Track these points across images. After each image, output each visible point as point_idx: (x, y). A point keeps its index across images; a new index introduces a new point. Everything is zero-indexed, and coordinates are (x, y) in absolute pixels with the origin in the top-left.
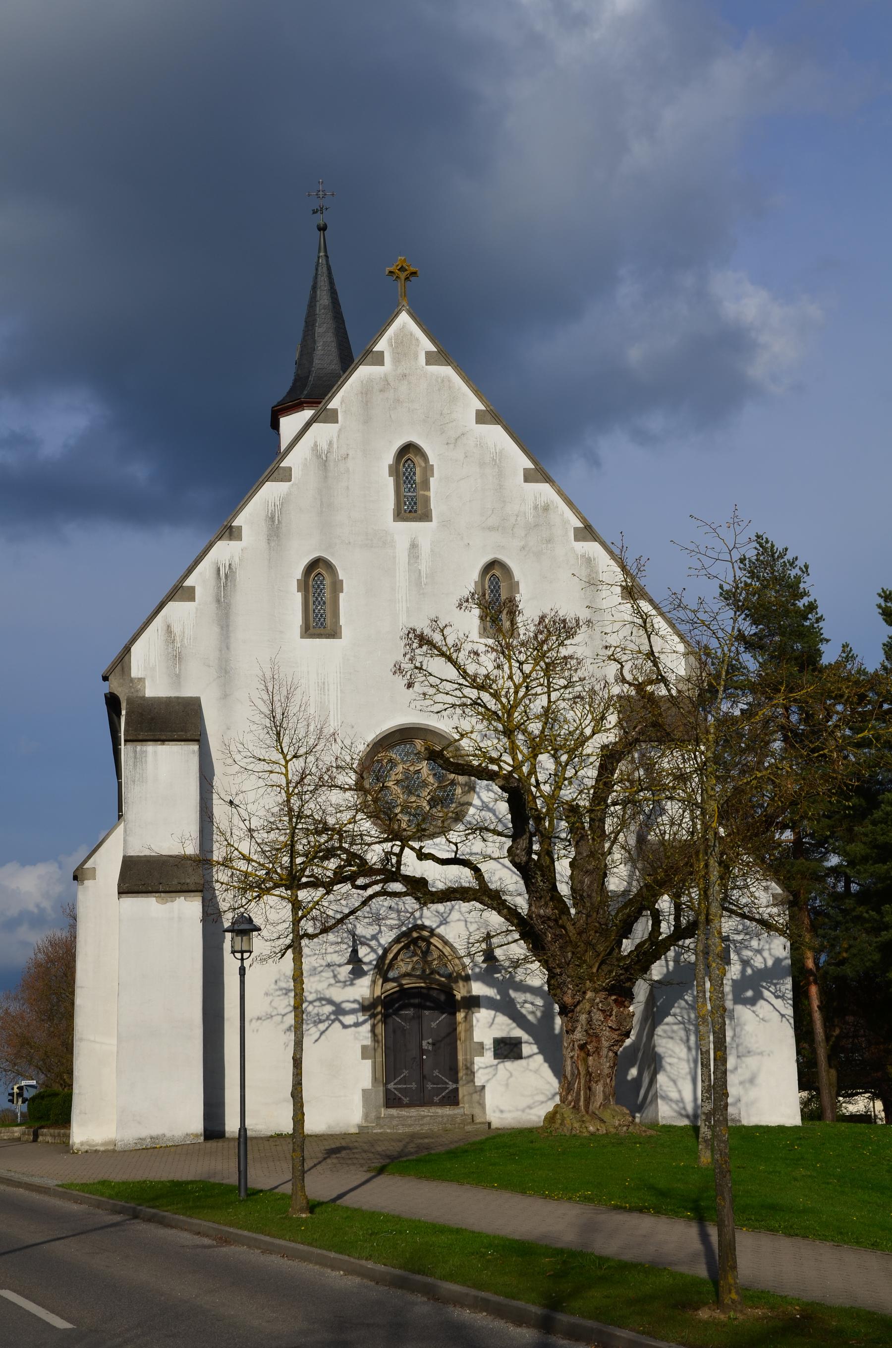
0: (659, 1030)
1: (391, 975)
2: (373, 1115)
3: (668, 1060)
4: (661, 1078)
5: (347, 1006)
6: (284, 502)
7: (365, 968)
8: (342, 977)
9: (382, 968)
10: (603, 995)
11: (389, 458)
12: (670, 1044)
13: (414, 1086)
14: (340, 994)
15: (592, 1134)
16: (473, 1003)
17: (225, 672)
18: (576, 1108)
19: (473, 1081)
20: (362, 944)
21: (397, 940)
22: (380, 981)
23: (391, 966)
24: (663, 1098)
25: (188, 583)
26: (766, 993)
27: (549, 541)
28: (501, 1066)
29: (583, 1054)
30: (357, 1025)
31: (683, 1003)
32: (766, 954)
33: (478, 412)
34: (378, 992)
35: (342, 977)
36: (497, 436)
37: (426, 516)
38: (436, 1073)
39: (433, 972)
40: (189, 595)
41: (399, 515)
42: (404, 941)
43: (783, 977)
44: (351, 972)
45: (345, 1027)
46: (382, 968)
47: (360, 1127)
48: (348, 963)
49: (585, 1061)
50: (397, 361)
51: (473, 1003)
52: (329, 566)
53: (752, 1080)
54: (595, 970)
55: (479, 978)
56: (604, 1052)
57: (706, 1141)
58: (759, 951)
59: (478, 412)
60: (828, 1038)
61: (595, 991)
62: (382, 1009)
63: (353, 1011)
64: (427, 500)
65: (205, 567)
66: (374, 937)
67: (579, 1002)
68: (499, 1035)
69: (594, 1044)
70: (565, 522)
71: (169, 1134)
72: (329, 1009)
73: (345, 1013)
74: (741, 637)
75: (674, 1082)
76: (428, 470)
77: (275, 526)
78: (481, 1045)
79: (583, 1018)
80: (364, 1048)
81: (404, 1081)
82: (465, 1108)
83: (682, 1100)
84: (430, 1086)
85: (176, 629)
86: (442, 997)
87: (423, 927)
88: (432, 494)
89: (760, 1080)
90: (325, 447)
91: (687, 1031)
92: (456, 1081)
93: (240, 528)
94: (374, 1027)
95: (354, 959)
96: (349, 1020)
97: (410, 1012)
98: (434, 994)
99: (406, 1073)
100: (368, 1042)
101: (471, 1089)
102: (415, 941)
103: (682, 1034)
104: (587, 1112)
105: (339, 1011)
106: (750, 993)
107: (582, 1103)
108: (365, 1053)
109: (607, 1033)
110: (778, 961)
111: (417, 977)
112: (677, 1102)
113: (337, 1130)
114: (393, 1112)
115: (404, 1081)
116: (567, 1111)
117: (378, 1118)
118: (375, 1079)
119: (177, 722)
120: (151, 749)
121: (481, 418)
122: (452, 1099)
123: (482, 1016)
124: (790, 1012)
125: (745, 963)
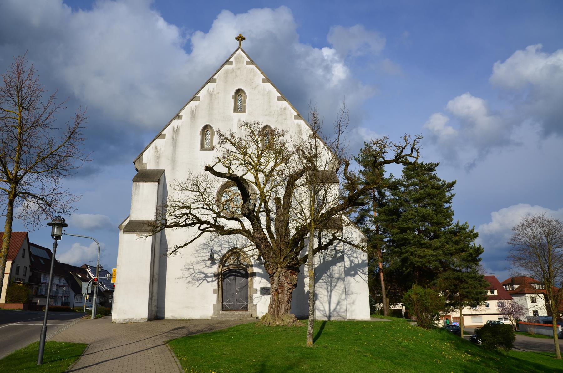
0: (317, 285)
1: (226, 265)
2: (216, 313)
3: (320, 296)
4: (317, 302)
5: (209, 275)
6: (197, 107)
7: (216, 262)
8: (208, 265)
9: (223, 262)
10: (285, 270)
11: (233, 93)
12: (321, 290)
13: (232, 303)
14: (206, 271)
15: (278, 326)
16: (254, 274)
17: (174, 161)
18: (273, 314)
19: (253, 302)
20: (216, 253)
21: (228, 252)
22: (221, 267)
23: (226, 261)
24: (317, 309)
25: (163, 133)
26: (359, 272)
27: (285, 119)
28: (263, 297)
29: (276, 293)
30: (212, 281)
31: (326, 275)
32: (359, 259)
33: (263, 79)
34: (220, 270)
35: (208, 265)
36: (269, 86)
37: (244, 111)
38: (241, 299)
39: (241, 264)
40: (164, 136)
41: (235, 111)
42: (230, 253)
43: (365, 267)
44: (211, 263)
45: (208, 282)
46: (223, 262)
47: (212, 317)
48: (209, 260)
49: (278, 296)
50: (237, 64)
51: (254, 274)
52: (211, 127)
53: (353, 303)
54: (282, 260)
55: (256, 266)
56: (286, 292)
57: (310, 334)
58: (356, 258)
59: (263, 79)
60: (386, 289)
61: (281, 268)
62: (222, 276)
63: (211, 277)
64: (245, 106)
65: (170, 128)
66: (220, 251)
67: (275, 273)
68: (263, 286)
69: (281, 289)
70: (291, 113)
71: (135, 318)
72: (203, 275)
73: (208, 277)
74: (360, 172)
75: (322, 304)
76: (246, 97)
77: (193, 115)
78: (256, 289)
79: (277, 279)
80: (214, 289)
81: (229, 301)
82: (250, 311)
83: (325, 310)
84: (238, 303)
85: (158, 147)
86: (244, 273)
87: (237, 248)
88: (246, 104)
89: (356, 303)
90: (212, 90)
91: (327, 285)
92: (247, 302)
93: (182, 115)
94: (218, 282)
95: (211, 258)
96: (210, 279)
97: (232, 278)
98: (241, 271)
99: (230, 299)
100: (216, 288)
101: (252, 305)
102: (234, 253)
103: (325, 286)
104: (278, 316)
105: (206, 276)
106: (353, 272)
107: (276, 313)
108: (215, 291)
109: (286, 285)
110: (363, 261)
111: (235, 265)
112: (323, 311)
113: (204, 318)
114: (224, 312)
115: (229, 301)
116: (269, 317)
117: (218, 314)
118: (218, 300)
119: (156, 176)
120: (142, 184)
121: (264, 81)
122: (246, 308)
123: (257, 279)
124: (367, 279)
125: (352, 262)
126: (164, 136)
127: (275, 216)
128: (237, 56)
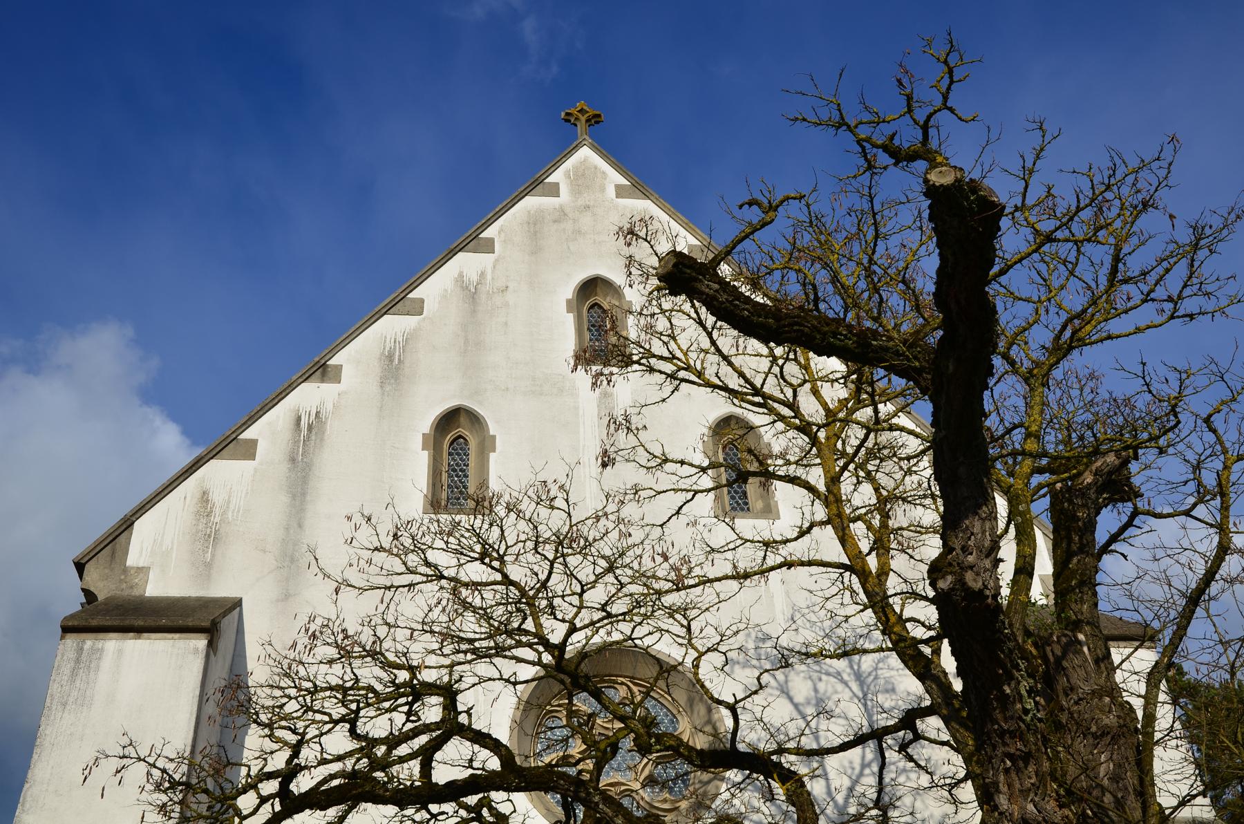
6: (409, 339)
25: (248, 434)
40: (249, 450)
76: (488, 444)
77: (393, 367)
85: (217, 497)
90: (475, 278)
93: (339, 368)
120: (112, 645)
126: (249, 450)
127: (379, 754)
128: (576, 168)
